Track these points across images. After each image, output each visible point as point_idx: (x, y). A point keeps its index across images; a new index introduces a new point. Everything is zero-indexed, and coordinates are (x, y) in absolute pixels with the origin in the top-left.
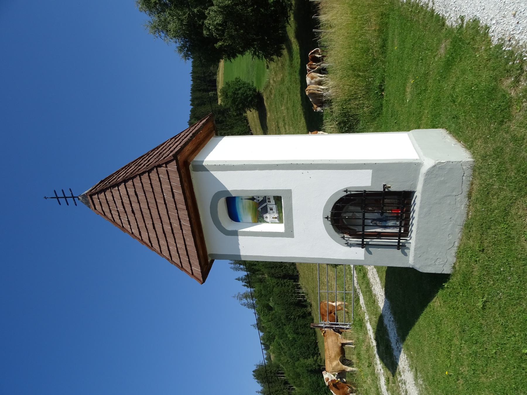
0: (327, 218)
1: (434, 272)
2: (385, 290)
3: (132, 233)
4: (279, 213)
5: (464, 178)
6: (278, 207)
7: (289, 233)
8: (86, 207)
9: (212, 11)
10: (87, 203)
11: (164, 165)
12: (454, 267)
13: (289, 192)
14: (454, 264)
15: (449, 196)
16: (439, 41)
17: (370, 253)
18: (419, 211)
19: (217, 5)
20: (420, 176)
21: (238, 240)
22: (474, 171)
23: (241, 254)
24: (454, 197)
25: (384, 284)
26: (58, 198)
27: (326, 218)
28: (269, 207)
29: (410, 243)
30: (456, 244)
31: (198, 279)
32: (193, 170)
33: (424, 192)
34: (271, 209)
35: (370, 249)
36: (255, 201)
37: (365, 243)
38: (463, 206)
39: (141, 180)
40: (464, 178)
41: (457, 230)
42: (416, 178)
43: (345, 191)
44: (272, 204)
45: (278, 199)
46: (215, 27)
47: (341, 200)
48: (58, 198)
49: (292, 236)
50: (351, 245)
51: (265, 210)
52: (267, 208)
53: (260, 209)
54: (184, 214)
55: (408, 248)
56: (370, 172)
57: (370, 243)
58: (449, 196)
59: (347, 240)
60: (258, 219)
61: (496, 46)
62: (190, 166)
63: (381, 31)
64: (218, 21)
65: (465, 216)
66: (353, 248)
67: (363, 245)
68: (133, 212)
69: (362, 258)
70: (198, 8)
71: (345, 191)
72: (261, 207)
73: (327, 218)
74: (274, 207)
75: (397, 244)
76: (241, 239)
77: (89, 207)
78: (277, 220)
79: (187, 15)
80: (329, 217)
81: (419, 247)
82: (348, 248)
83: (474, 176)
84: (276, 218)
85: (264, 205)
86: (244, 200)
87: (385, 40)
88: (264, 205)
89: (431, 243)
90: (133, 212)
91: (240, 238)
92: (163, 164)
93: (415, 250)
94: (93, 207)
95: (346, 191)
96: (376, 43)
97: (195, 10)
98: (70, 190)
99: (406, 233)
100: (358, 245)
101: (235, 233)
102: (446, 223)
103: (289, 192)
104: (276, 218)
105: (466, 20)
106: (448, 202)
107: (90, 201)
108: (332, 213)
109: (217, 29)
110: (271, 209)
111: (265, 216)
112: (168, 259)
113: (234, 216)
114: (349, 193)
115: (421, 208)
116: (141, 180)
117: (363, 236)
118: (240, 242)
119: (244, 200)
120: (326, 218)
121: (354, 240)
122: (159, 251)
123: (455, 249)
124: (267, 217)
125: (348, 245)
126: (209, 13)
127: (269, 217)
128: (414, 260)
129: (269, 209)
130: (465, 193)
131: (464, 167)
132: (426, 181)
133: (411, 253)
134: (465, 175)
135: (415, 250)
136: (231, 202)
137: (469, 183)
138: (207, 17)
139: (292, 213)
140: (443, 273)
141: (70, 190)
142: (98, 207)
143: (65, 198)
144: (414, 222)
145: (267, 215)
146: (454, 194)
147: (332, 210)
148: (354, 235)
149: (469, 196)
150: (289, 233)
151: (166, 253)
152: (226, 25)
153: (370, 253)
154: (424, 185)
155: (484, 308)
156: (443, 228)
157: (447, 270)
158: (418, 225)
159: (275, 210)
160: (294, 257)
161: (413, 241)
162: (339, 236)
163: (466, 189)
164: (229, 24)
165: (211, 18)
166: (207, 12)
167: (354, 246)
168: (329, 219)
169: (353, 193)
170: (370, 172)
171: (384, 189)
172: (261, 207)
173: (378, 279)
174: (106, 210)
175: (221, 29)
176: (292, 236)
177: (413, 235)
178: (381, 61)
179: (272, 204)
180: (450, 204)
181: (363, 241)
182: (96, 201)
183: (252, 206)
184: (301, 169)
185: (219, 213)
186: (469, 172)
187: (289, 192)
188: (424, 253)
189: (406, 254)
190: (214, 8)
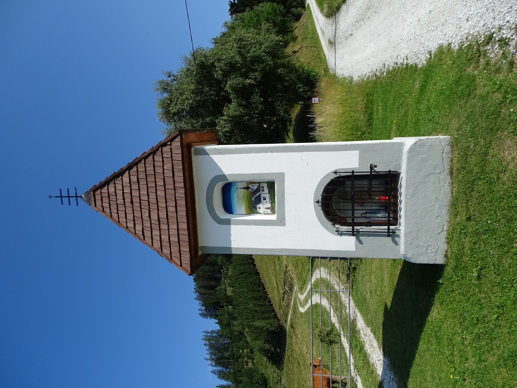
0: (318, 202)
1: (426, 262)
2: (384, 351)
3: (127, 227)
4: (272, 203)
5: (444, 155)
6: (271, 196)
7: (281, 222)
8: (87, 205)
9: (223, 120)
10: (88, 201)
11: (169, 143)
12: (446, 256)
13: (282, 175)
14: (446, 252)
15: (432, 174)
16: (415, 80)
17: (361, 242)
18: (406, 192)
19: (227, 115)
20: (403, 156)
21: (230, 230)
22: (452, 146)
23: (232, 246)
24: (437, 175)
25: (381, 341)
26: (61, 197)
27: (317, 202)
28: (263, 196)
29: (400, 230)
30: (446, 228)
31: (187, 271)
32: (195, 154)
33: (408, 170)
34: (265, 199)
35: (361, 238)
36: (250, 190)
37: (355, 230)
38: (447, 184)
39: (145, 163)
40: (444, 155)
41: (445, 211)
42: (400, 159)
43: (334, 173)
44: (265, 194)
45: (271, 185)
46: (223, 133)
47: (332, 183)
48: (61, 197)
49: (284, 225)
50: (341, 234)
51: (258, 200)
52: (260, 198)
53: (253, 199)
54: (181, 193)
55: (398, 236)
56: (357, 152)
57: (360, 230)
58: (432, 174)
59: (337, 228)
60: (251, 209)
61: (457, 50)
62: (193, 149)
63: (367, 107)
64: (227, 129)
65: (450, 195)
66: (343, 237)
67: (353, 233)
68: (132, 202)
69: (353, 249)
70: (211, 118)
71: (334, 173)
72: (255, 197)
73: (318, 202)
74: (268, 196)
75: (387, 231)
76: (234, 228)
77: (90, 205)
78: (269, 211)
79: (200, 123)
80: (320, 201)
81: (410, 233)
82: (339, 237)
83: (452, 151)
84: (268, 208)
85: (258, 194)
86: (239, 190)
87: (371, 114)
88: (258, 194)
89: (422, 230)
90: (132, 202)
91: (233, 227)
92: (168, 142)
93: (406, 235)
94: (94, 204)
95: (335, 172)
96: (362, 118)
97: (208, 120)
98: (76, 189)
99: (395, 221)
100: (347, 233)
101: (228, 222)
102: (432, 204)
103: (282, 175)
104: (268, 208)
105: (433, 52)
106: (432, 180)
107: (93, 199)
108: (322, 196)
109: (225, 136)
110: (265, 199)
111: (258, 206)
112: (158, 252)
113: (228, 208)
114: (338, 175)
115: (407, 188)
116: (145, 163)
117: (353, 224)
118: (232, 232)
119: (239, 190)
120: (317, 202)
121: (344, 228)
122: (151, 244)
123: (444, 234)
124: (260, 208)
125: (339, 234)
126: (219, 122)
127: (263, 207)
128: (405, 248)
129: (262, 199)
130: (447, 171)
131: (443, 144)
132: (409, 158)
133: (402, 241)
134: (444, 152)
135: (405, 237)
136: (227, 189)
137: (449, 159)
138: (217, 124)
139: (284, 198)
140: (436, 263)
141: (76, 189)
142: (99, 203)
143: (69, 197)
144: (401, 214)
145: (260, 205)
146: (437, 171)
147: (323, 193)
148: (344, 223)
149: (451, 173)
150: (281, 222)
151: (157, 245)
152: (233, 133)
153: (361, 242)
154: (408, 163)
155: (479, 277)
156: (430, 209)
157: (440, 260)
158: (405, 207)
159: (268, 200)
160: (285, 249)
161: (402, 228)
162: (329, 224)
163: (447, 167)
164: (236, 132)
165: (221, 126)
166: (217, 121)
167: (345, 235)
168: (320, 204)
169: (342, 174)
170: (357, 152)
171: (371, 172)
172: (255, 197)
173: (375, 344)
174: (106, 205)
175: (228, 136)
176: (284, 225)
177: (402, 220)
178: (368, 132)
179: (265, 194)
180: (434, 183)
181: (353, 229)
182: (98, 197)
183: (246, 195)
184: (294, 152)
185: (214, 199)
186: (448, 149)
187: (282, 175)
188: (414, 239)
189: (396, 243)
190: (225, 118)
